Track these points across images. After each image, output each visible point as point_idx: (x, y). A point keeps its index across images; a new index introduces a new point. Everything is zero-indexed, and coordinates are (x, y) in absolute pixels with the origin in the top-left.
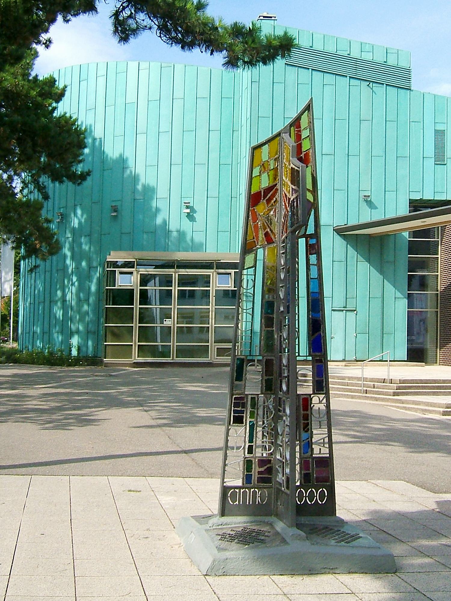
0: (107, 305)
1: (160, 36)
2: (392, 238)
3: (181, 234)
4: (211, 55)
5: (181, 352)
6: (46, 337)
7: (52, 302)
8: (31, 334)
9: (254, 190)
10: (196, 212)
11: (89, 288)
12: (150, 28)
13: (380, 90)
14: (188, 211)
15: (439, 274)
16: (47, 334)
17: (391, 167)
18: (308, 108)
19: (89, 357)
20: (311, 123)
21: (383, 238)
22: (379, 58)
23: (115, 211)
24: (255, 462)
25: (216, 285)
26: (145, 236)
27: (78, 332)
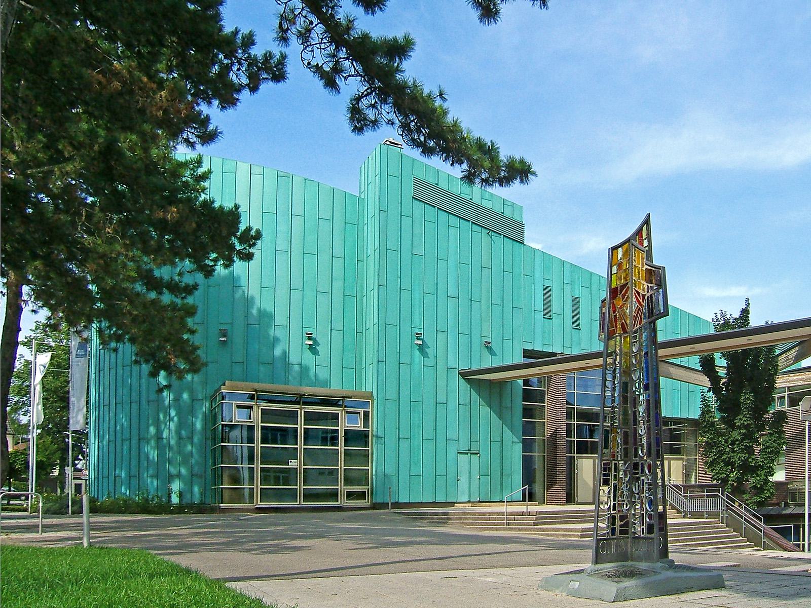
0: (222, 442)
1: (402, 135)
2: (509, 386)
3: (304, 369)
4: (451, 166)
5: (308, 496)
6: (134, 482)
7: (142, 439)
8: (112, 478)
9: (614, 285)
10: (319, 345)
11: (193, 424)
12: (393, 124)
13: (498, 240)
14: (311, 342)
15: (546, 421)
16: (134, 478)
17: (508, 316)
18: (647, 222)
19: (195, 504)
20: (649, 234)
21: (502, 383)
22: (498, 208)
23: (224, 336)
24: (618, 516)
25: (345, 424)
26: (262, 368)
27: (179, 476)
